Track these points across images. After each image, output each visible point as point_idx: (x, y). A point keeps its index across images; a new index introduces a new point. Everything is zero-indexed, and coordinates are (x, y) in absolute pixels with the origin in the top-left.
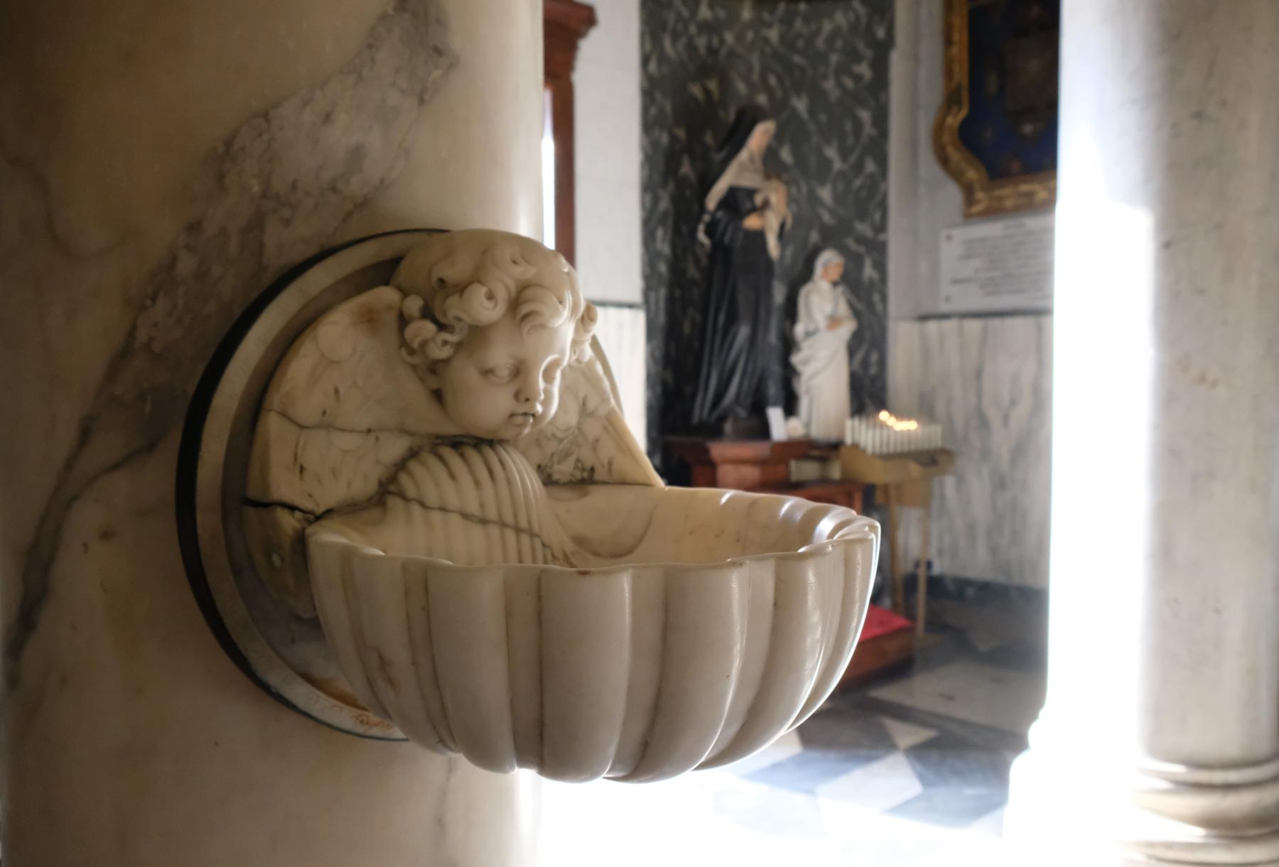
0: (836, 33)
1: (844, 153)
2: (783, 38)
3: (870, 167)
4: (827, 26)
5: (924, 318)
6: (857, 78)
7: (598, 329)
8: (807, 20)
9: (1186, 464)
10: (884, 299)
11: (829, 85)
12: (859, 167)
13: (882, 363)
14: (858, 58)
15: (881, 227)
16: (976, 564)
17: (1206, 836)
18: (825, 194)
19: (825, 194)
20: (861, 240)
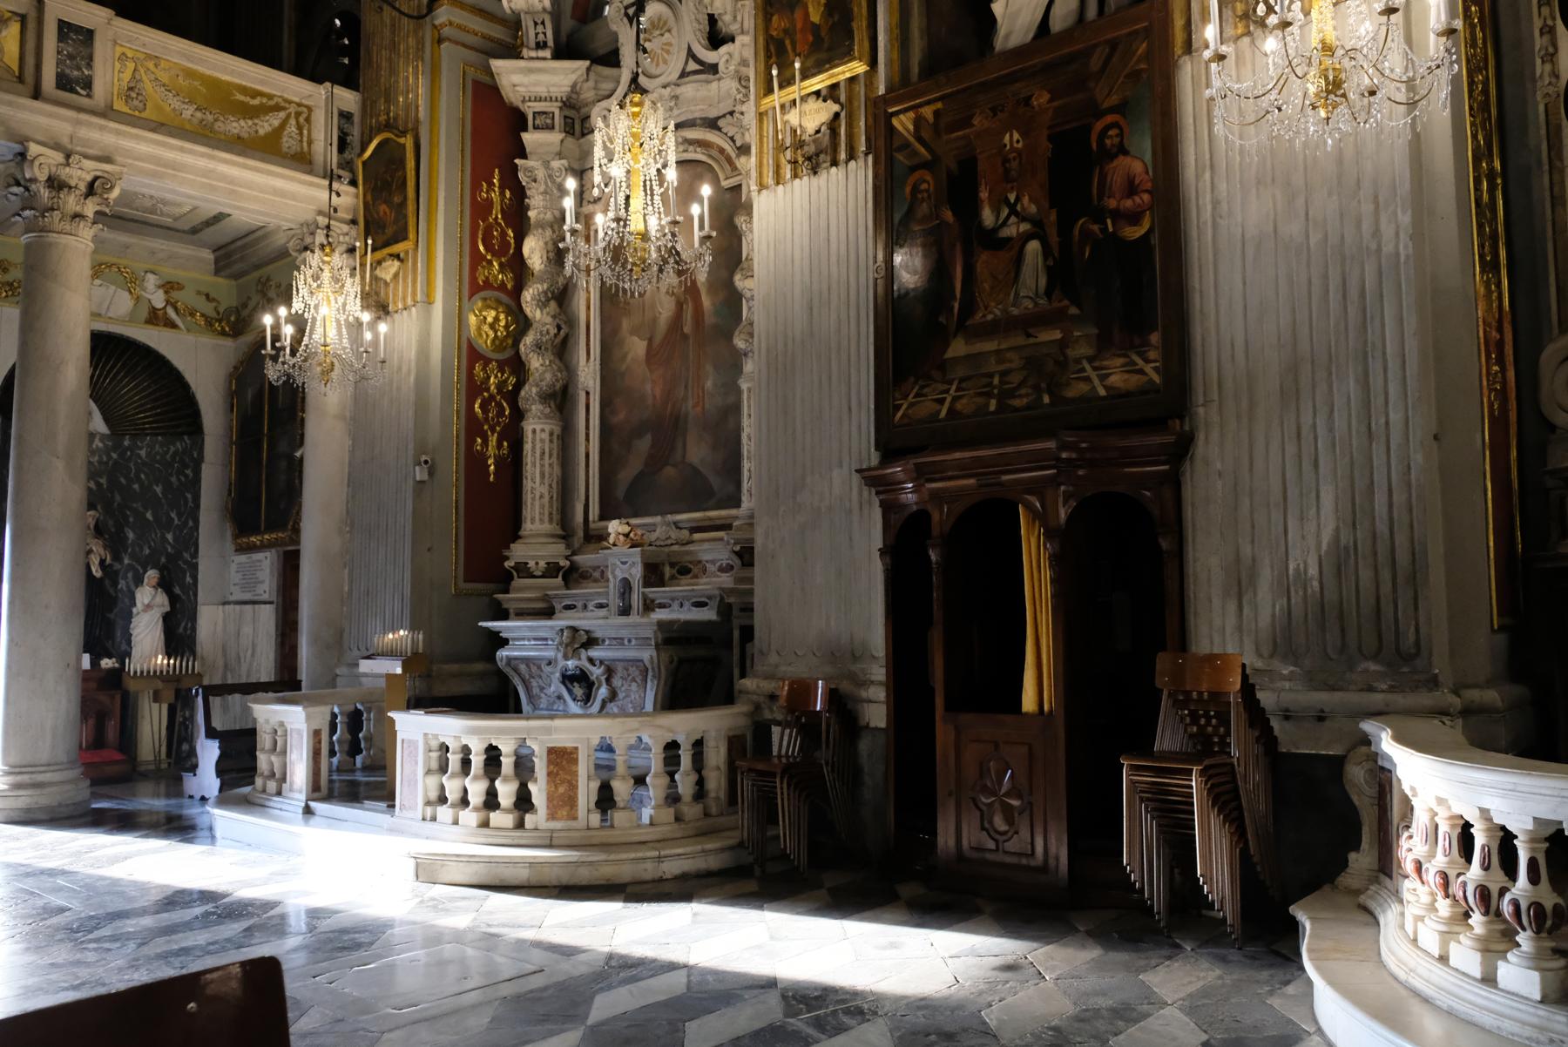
0: (176, 453)
1: (179, 515)
2: (148, 454)
3: (191, 523)
4: (172, 449)
5: (224, 604)
6: (186, 476)
7: (1093, 1042)
8: (162, 446)
9: (715, 993)
10: (196, 595)
11: (174, 479)
12: (185, 524)
13: (194, 629)
14: (187, 467)
15: (195, 554)
16: (250, 726)
17: (1098, 966)
18: (170, 537)
19: (170, 537)
20: (186, 562)
